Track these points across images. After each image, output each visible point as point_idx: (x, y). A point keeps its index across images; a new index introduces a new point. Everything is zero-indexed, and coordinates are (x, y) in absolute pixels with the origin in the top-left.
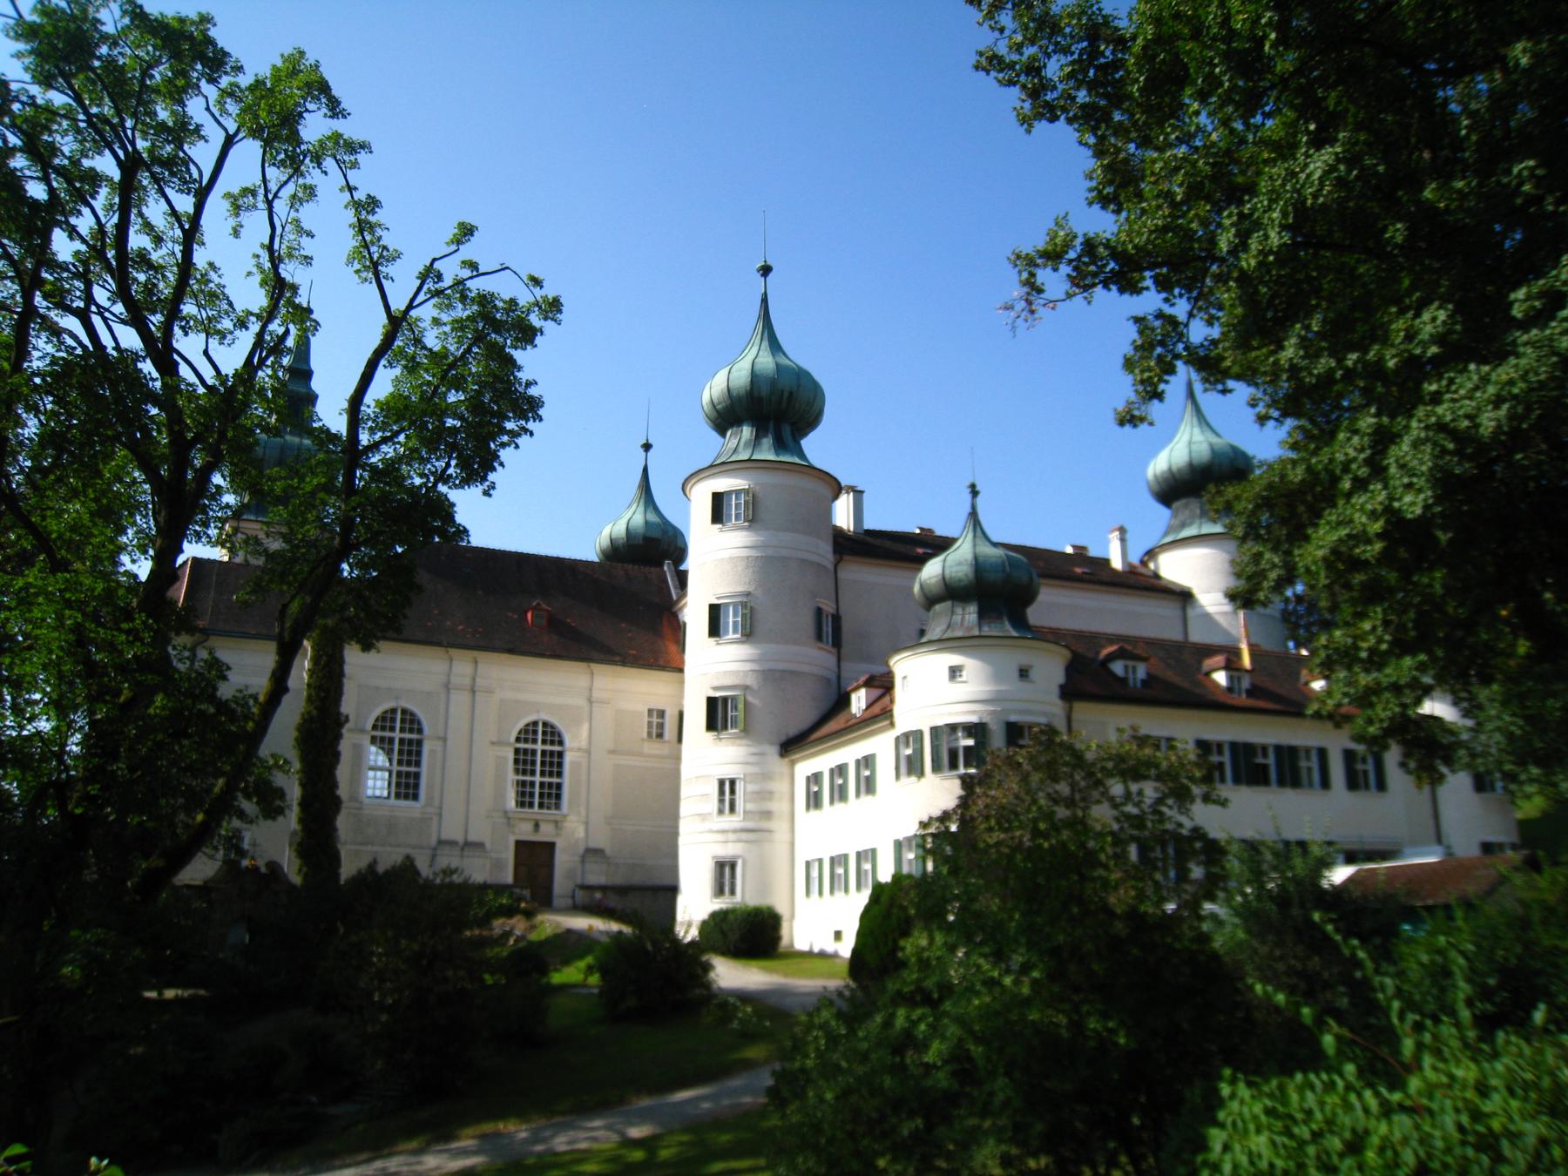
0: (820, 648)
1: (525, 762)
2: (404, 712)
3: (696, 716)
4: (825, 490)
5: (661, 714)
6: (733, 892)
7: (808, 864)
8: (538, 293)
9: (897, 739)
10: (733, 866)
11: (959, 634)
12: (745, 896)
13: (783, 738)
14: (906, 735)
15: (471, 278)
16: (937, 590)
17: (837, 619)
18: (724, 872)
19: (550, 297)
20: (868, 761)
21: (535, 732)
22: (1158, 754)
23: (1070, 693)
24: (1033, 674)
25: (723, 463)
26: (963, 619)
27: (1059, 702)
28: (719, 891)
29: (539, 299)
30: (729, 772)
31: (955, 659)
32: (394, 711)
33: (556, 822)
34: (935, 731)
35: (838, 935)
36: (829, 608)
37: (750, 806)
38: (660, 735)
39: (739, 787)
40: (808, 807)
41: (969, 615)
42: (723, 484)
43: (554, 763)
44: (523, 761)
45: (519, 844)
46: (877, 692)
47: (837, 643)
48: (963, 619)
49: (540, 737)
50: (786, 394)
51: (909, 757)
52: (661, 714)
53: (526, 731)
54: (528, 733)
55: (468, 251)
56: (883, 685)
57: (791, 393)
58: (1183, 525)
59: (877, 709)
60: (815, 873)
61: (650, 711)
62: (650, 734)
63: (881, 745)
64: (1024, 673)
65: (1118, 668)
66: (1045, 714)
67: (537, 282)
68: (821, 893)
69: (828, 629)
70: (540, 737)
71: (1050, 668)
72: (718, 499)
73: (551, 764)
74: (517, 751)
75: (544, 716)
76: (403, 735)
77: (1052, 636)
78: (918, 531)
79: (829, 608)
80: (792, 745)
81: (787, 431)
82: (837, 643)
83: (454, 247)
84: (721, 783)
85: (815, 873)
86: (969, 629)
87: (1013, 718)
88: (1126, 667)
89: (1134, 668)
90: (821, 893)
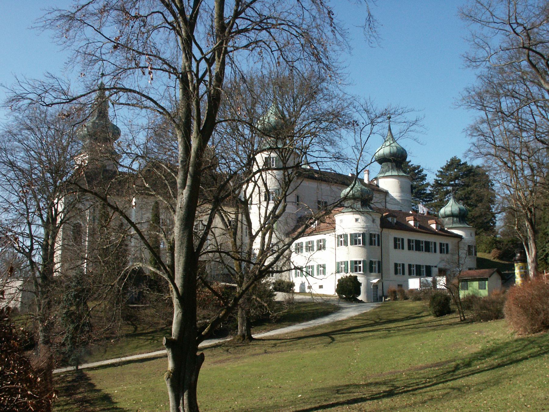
14: (341, 236)
27: (379, 228)
34: (351, 235)
58: (386, 171)
64: (357, 220)
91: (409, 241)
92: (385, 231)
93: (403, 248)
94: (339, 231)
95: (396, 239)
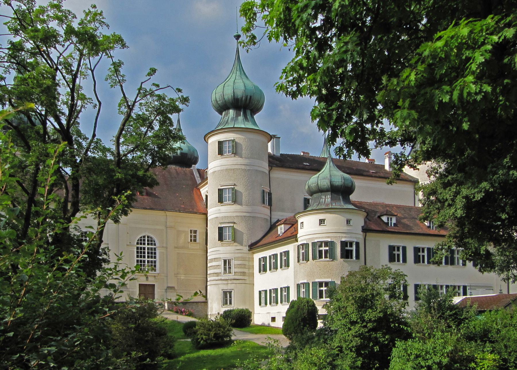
0: (264, 207)
1: (141, 253)
2: (148, 237)
3: (213, 234)
4: (263, 139)
5: (195, 232)
6: (231, 303)
7: (260, 292)
8: (180, 94)
9: (298, 246)
10: (230, 293)
11: (324, 207)
12: (236, 305)
13: (250, 244)
15: (157, 90)
16: (314, 189)
17: (270, 194)
18: (227, 296)
19: (185, 97)
20: (287, 253)
21: (144, 240)
22: (470, 78)
23: (366, 230)
24: (351, 222)
25: (222, 129)
26: (325, 200)
27: (361, 233)
28: (225, 303)
29: (180, 96)
30: (227, 257)
31: (322, 216)
32: (144, 237)
33: (155, 276)
34: (314, 244)
35: (273, 319)
36: (267, 190)
37: (237, 270)
38: (195, 241)
39: (233, 263)
40: (260, 272)
41: (327, 198)
42: (221, 137)
43: (152, 253)
44: (140, 252)
45: (140, 285)
46: (288, 226)
47: (270, 204)
48: (325, 200)
49: (146, 242)
50: (249, 97)
51: (303, 253)
52: (195, 232)
53: (141, 240)
54: (141, 241)
55: (154, 79)
56: (293, 224)
57: (251, 97)
59: (289, 234)
60: (263, 295)
61: (191, 231)
62: (191, 241)
63: (291, 248)
64: (348, 222)
65: (385, 219)
66: (356, 238)
67: (179, 90)
68: (266, 304)
69: (267, 198)
70: (146, 242)
71: (359, 221)
72: (220, 144)
73: (152, 253)
74: (137, 248)
75: (147, 234)
76: (144, 246)
77: (359, 207)
78: (302, 154)
79: (267, 190)
80: (253, 247)
81: (248, 112)
82: (270, 204)
83: (149, 77)
84: (225, 261)
85: (263, 295)
86: (327, 205)
87: (343, 240)
88: (388, 219)
89: (391, 219)
90: (266, 304)
91: (417, 250)
92: (371, 236)
93: (405, 261)
94: (301, 240)
95: (392, 249)
